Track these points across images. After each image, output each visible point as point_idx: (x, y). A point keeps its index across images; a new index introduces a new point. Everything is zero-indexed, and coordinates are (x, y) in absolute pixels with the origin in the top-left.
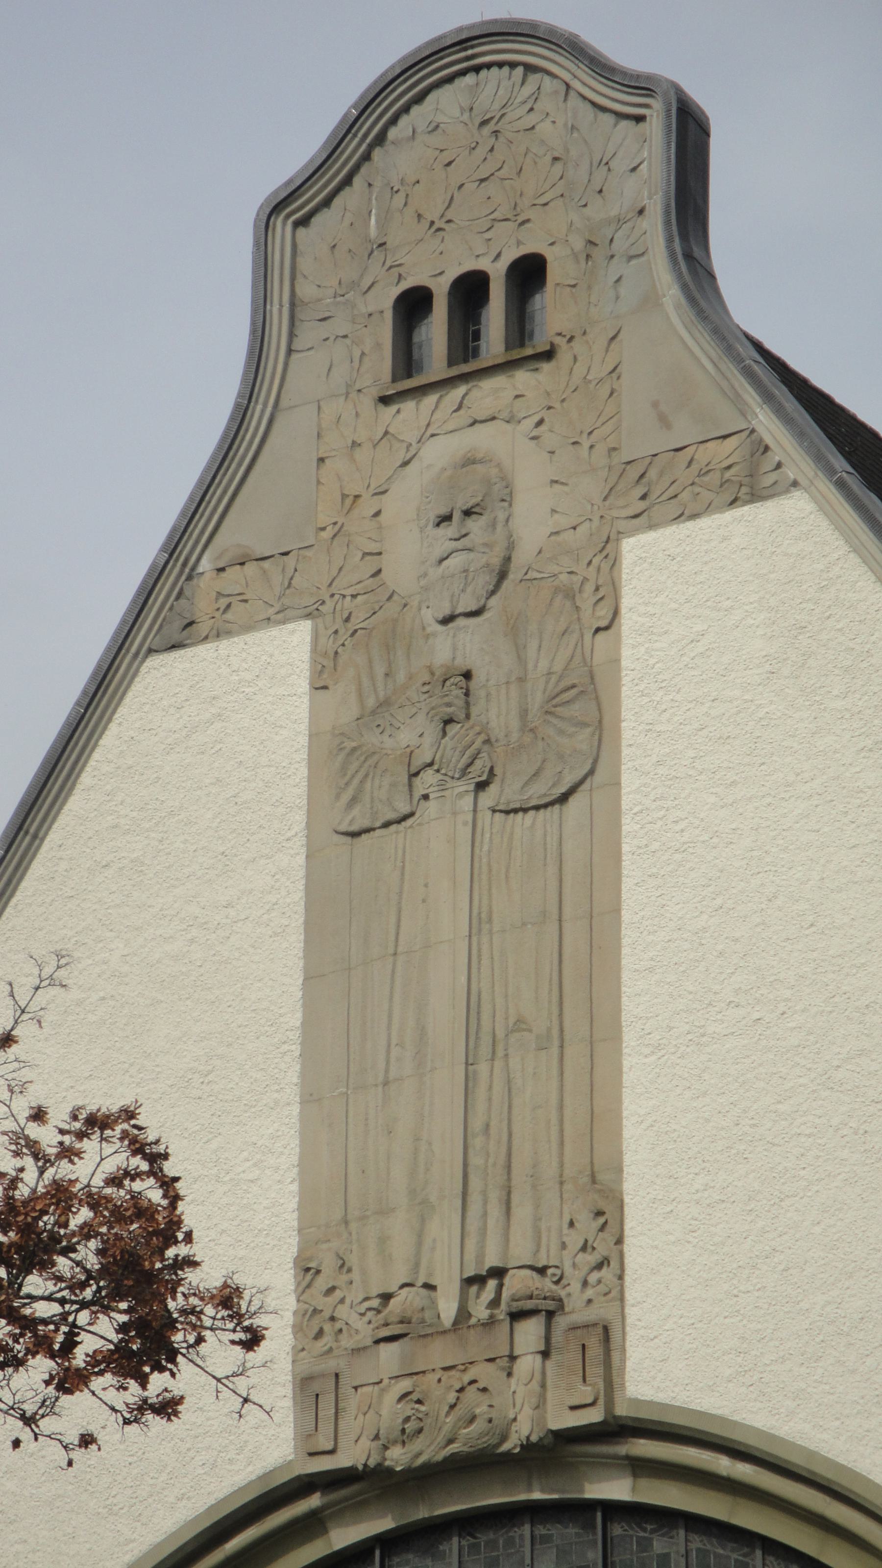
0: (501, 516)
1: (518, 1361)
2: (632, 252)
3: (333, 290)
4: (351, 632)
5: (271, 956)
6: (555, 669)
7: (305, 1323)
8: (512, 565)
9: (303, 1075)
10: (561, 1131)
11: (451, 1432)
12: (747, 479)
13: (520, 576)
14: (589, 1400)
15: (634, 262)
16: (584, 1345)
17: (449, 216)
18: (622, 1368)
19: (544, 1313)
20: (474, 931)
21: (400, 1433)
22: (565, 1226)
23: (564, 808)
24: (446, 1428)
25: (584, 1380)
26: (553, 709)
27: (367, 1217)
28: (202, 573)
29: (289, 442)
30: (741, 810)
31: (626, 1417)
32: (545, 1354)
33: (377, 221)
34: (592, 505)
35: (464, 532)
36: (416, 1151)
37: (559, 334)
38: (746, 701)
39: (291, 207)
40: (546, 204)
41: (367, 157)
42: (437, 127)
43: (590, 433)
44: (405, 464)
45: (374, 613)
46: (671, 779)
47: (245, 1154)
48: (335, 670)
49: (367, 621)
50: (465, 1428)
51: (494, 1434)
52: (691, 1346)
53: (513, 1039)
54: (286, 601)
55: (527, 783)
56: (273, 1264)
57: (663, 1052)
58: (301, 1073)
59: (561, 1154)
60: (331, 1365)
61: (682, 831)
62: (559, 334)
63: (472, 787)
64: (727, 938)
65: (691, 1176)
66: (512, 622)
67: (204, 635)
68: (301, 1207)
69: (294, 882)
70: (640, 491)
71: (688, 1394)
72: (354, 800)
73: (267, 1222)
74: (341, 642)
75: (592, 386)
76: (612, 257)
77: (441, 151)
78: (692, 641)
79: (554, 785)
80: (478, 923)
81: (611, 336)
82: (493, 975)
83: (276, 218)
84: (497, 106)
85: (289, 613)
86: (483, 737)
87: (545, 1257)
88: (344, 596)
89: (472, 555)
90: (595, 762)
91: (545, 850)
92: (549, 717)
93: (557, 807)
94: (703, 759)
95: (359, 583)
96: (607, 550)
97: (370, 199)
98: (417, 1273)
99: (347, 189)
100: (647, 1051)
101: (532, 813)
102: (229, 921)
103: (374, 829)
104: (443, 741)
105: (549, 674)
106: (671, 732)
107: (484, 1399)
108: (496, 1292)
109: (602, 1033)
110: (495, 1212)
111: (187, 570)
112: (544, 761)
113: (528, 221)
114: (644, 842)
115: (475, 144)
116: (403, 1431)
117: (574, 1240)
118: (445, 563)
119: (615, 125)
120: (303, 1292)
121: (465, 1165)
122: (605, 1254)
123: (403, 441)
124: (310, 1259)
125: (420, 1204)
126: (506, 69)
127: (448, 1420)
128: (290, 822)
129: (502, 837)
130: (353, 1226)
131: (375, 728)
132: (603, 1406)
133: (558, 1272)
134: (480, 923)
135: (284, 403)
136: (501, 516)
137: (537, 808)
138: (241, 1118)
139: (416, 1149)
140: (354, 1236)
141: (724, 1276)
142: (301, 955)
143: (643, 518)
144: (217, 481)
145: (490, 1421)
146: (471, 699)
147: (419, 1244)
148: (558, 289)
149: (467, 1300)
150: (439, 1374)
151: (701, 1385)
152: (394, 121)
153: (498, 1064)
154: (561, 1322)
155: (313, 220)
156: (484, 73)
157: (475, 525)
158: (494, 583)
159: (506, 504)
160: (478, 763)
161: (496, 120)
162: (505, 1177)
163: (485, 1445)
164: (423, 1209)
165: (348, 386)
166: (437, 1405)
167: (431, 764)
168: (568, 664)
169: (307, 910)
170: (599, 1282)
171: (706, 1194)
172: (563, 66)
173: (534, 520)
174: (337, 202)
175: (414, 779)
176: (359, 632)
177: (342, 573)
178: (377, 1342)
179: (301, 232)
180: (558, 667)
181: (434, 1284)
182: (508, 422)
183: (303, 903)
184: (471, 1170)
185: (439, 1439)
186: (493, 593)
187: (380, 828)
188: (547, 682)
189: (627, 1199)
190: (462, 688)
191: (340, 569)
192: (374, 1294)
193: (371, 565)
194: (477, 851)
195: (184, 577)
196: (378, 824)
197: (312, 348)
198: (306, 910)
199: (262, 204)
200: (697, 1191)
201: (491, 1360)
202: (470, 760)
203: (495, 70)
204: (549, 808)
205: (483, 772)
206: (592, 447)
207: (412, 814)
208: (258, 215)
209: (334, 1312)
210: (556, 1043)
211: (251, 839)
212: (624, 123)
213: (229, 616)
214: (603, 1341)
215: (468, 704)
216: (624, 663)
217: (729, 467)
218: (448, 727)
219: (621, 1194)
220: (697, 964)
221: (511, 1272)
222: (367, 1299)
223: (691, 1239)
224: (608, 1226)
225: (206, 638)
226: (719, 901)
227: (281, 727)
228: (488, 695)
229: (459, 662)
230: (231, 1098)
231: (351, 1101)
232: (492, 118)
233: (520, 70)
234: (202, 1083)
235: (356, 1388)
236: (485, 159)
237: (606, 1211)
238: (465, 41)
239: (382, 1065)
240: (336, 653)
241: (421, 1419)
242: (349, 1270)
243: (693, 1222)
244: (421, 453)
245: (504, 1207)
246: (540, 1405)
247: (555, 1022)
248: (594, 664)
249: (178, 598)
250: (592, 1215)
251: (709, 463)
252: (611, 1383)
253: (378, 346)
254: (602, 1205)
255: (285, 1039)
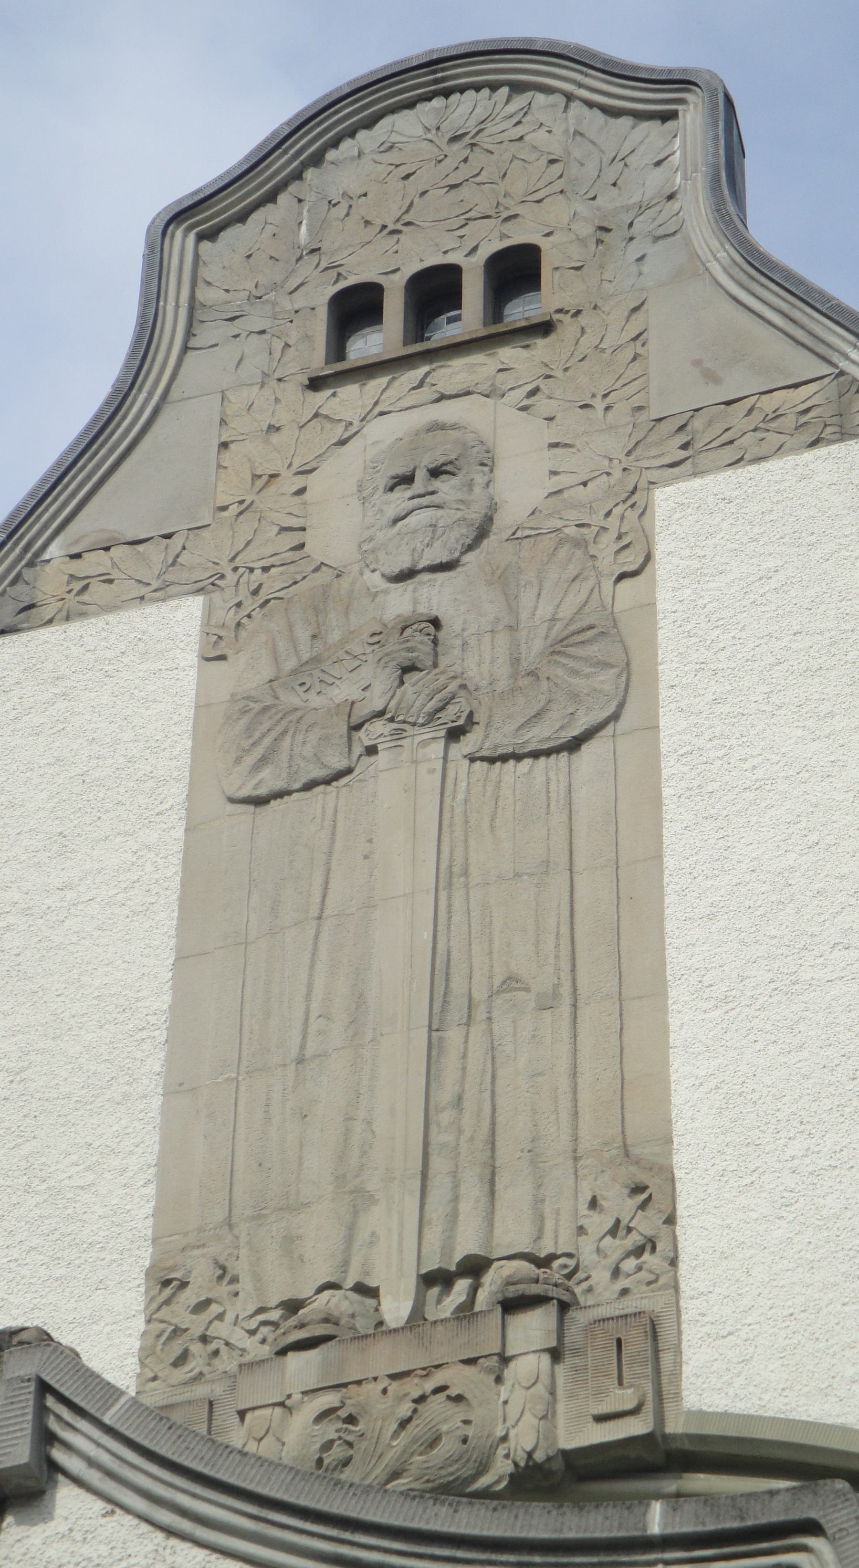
0: (480, 480)
1: (512, 1365)
2: (661, 232)
3: (247, 293)
4: (262, 601)
5: (128, 937)
6: (560, 615)
7: (159, 1347)
8: (494, 527)
9: (169, 1062)
10: (575, 1100)
11: (397, 1460)
12: (835, 420)
13: (507, 534)
14: (629, 1406)
15: (661, 242)
16: (619, 1342)
17: (407, 218)
18: (677, 1374)
19: (555, 1301)
20: (442, 885)
21: (314, 1464)
22: (583, 1209)
23: (574, 757)
24: (390, 1455)
25: (620, 1383)
26: (563, 649)
27: (265, 1216)
28: (48, 561)
29: (178, 445)
30: (842, 742)
31: (683, 1435)
32: (556, 1354)
33: (309, 230)
34: (611, 460)
35: (430, 489)
36: (347, 1133)
37: (560, 311)
38: (845, 631)
39: (201, 216)
40: (539, 201)
41: (297, 176)
42: (391, 147)
43: (605, 396)
44: (343, 442)
45: (295, 583)
46: (735, 717)
47: (74, 1158)
48: (237, 640)
49: (285, 591)
50: (421, 1454)
51: (468, 1460)
52: (787, 1342)
53: (498, 1001)
54: (170, 577)
55: (519, 728)
56: (109, 1283)
57: (731, 1006)
58: (165, 1061)
59: (575, 1127)
60: (202, 1391)
61: (754, 767)
62: (560, 311)
63: (443, 733)
64: (827, 876)
65: (782, 1141)
66: (499, 572)
67: (48, 618)
68: (158, 1213)
69: (165, 858)
70: (682, 439)
71: (786, 1400)
72: (263, 761)
73: (102, 1233)
74: (247, 613)
75: (606, 355)
76: (631, 239)
77: (397, 166)
78: (761, 578)
79: (562, 728)
80: (449, 877)
81: (632, 307)
82: (470, 932)
83: (176, 228)
84: (472, 122)
85: (171, 590)
86: (458, 682)
87: (552, 1243)
88: (252, 570)
89: (440, 512)
90: (621, 705)
91: (548, 798)
92: (556, 657)
93: (564, 756)
94: (781, 693)
95: (272, 556)
96: (635, 499)
97: (300, 214)
98: (346, 1272)
99: (270, 206)
100: (706, 1005)
101: (528, 762)
102: (66, 904)
103: (289, 793)
104: (399, 692)
105: (553, 619)
106: (733, 669)
107: (458, 1413)
108: (468, 1295)
109: (638, 990)
110: (472, 1191)
111: (29, 555)
112: (549, 701)
113: (516, 216)
114: (696, 783)
115: (443, 157)
116: (320, 1462)
117: (599, 1223)
118: (400, 524)
119: (633, 127)
120: (159, 1309)
121: (426, 1144)
122: (649, 1233)
123: (340, 420)
124: (173, 1269)
125: (352, 1192)
126: (486, 92)
127: (395, 1443)
128: (163, 796)
129: (484, 786)
130: (243, 1230)
131: (298, 688)
132: (651, 1413)
133: (572, 1263)
134: (451, 877)
135: (174, 394)
136: (480, 480)
137: (536, 755)
138: (68, 1117)
139: (347, 1130)
140: (244, 1238)
141: (840, 1255)
142: (173, 932)
143: (687, 459)
144: (79, 465)
145: (465, 1441)
146: (440, 649)
147: (349, 1240)
148: (557, 274)
149: (424, 1304)
150: (386, 1382)
151: (808, 1388)
152: (335, 143)
153: (477, 1031)
154: (579, 1318)
155: (222, 234)
156: (455, 97)
157: (445, 487)
158: (472, 537)
159: (486, 469)
160: (452, 710)
161: (472, 134)
162: (489, 1153)
163: (451, 1478)
164: (357, 1200)
165: (265, 375)
166: (379, 1423)
167: (381, 714)
168: (581, 608)
169: (184, 884)
170: (639, 1269)
171: (807, 1161)
172: (565, 78)
173: (520, 484)
174: (256, 218)
175: (354, 733)
176: (272, 601)
177: (250, 548)
178: (282, 1352)
179: (206, 245)
180: (566, 612)
181: (373, 1284)
182: (487, 396)
183: (179, 879)
184: (434, 1149)
185: (377, 1471)
186: (470, 548)
187: (298, 791)
188: (550, 629)
189: (678, 1174)
190: (429, 634)
191: (248, 543)
192: (274, 1302)
193: (294, 539)
194: (448, 801)
195: (23, 563)
196: (297, 786)
197: (216, 345)
198: (182, 886)
199: (160, 212)
200: (793, 1158)
201: (470, 1361)
202: (441, 704)
203: (470, 94)
204: (553, 757)
205: (459, 717)
206: (607, 409)
207: (349, 771)
208: (153, 222)
209: (207, 1329)
210: (567, 1001)
211: (104, 817)
212: (646, 125)
213: (85, 597)
214: (647, 1342)
215: (436, 655)
216: (660, 606)
217: (807, 411)
218: (406, 677)
219: (671, 1167)
220: (781, 907)
221: (496, 1265)
222: (261, 1310)
223: (784, 1214)
224: (651, 1204)
225: (50, 622)
226: (814, 837)
227: (155, 701)
228: (465, 644)
229: (422, 609)
230: (55, 1096)
231: (242, 1088)
232: (466, 134)
233: (505, 91)
234: (12, 1081)
235: (242, 1414)
236: (457, 168)
237: (647, 1183)
238: (433, 63)
239: (296, 1041)
240: (239, 624)
241: (350, 1445)
242: (234, 1280)
243: (786, 1194)
244: (365, 430)
245: (487, 1186)
246: (548, 1416)
247: (566, 976)
248: (616, 610)
249: (14, 582)
250: (626, 1191)
251: (778, 409)
252: (661, 1395)
253: (308, 338)
254: (642, 1177)
255: (145, 1024)
